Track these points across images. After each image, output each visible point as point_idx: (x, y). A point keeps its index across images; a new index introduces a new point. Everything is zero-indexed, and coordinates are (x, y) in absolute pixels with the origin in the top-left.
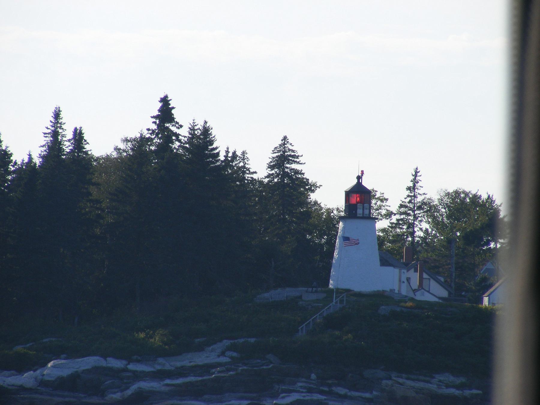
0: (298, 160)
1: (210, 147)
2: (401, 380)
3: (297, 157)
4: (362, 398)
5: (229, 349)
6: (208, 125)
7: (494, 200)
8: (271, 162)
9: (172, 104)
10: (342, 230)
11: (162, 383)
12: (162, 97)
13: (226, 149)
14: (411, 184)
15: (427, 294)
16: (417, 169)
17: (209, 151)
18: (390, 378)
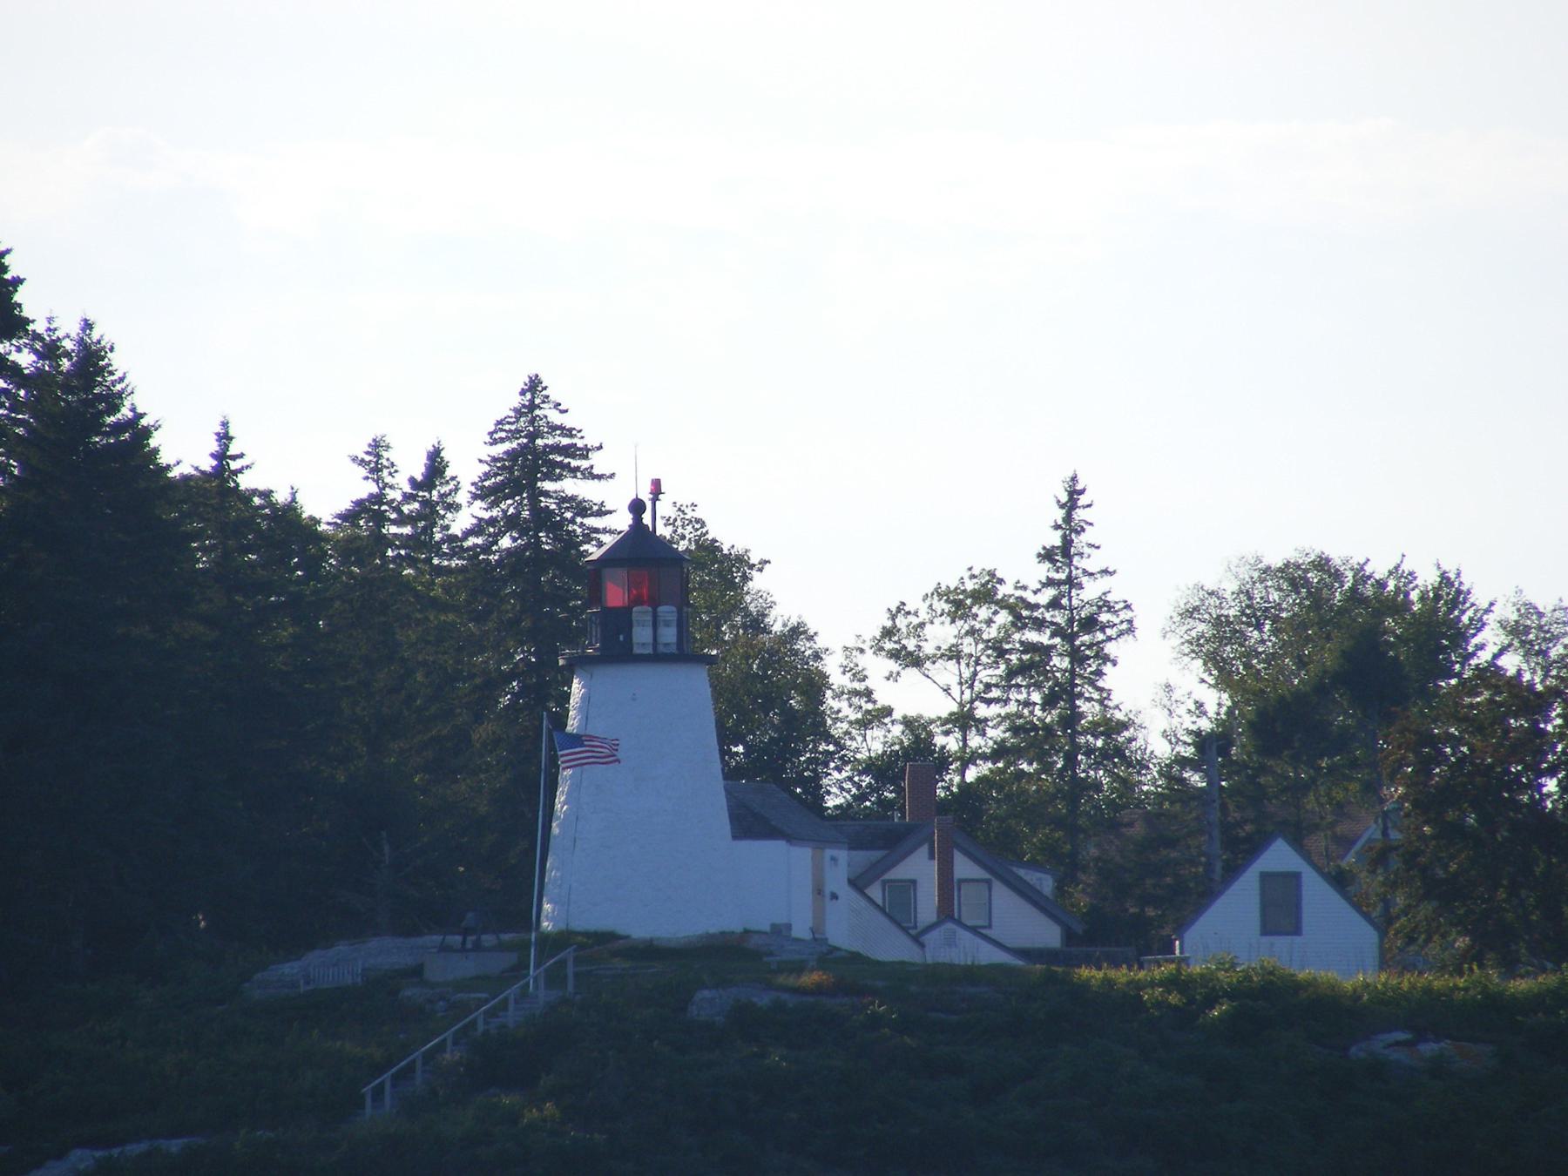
0: (584, 464)
1: (111, 420)
3: (584, 453)
6: (95, 336)
7: (1464, 588)
8: (487, 476)
10: (580, 709)
13: (219, 429)
14: (1055, 539)
15: (965, 937)
16: (1074, 479)
17: (107, 434)
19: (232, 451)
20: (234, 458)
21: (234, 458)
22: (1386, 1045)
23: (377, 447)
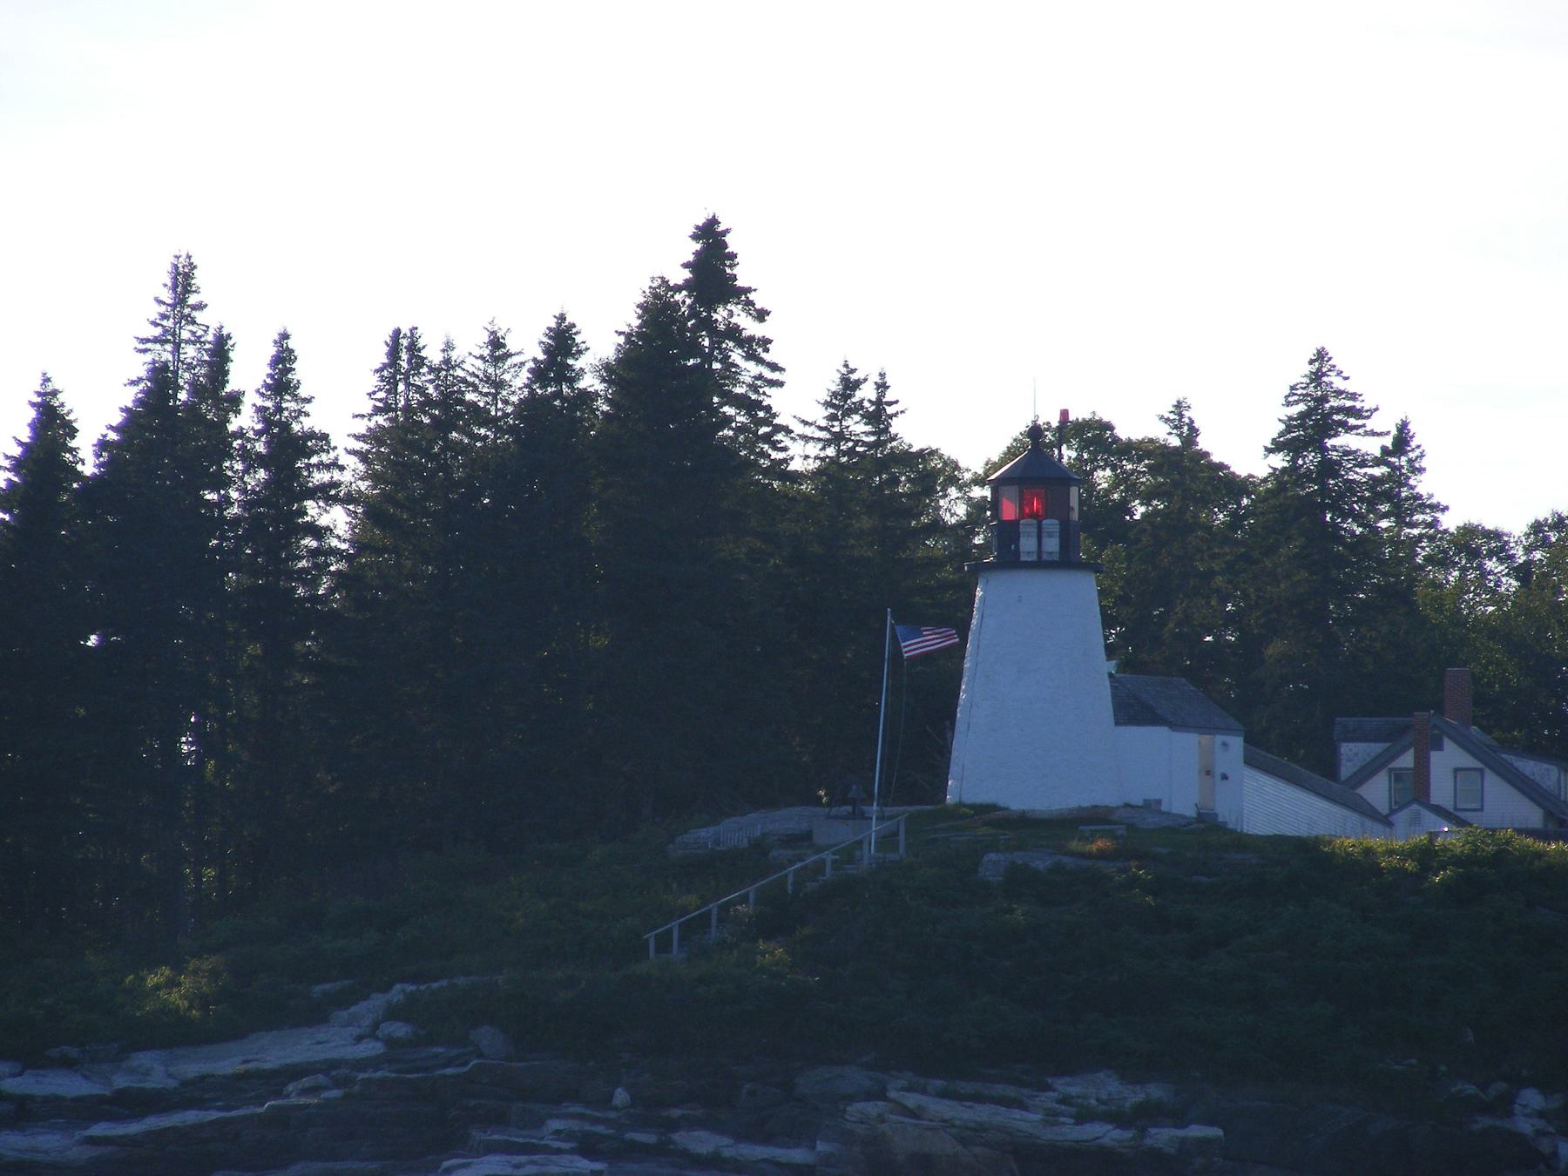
2: (912, 1100)
4: (778, 1164)
5: (393, 1013)
8: (1281, 434)
9: (733, 243)
11: (79, 1134)
18: (881, 1095)
19: (888, 398)
20: (890, 404)
21: (890, 404)
23: (1179, 407)
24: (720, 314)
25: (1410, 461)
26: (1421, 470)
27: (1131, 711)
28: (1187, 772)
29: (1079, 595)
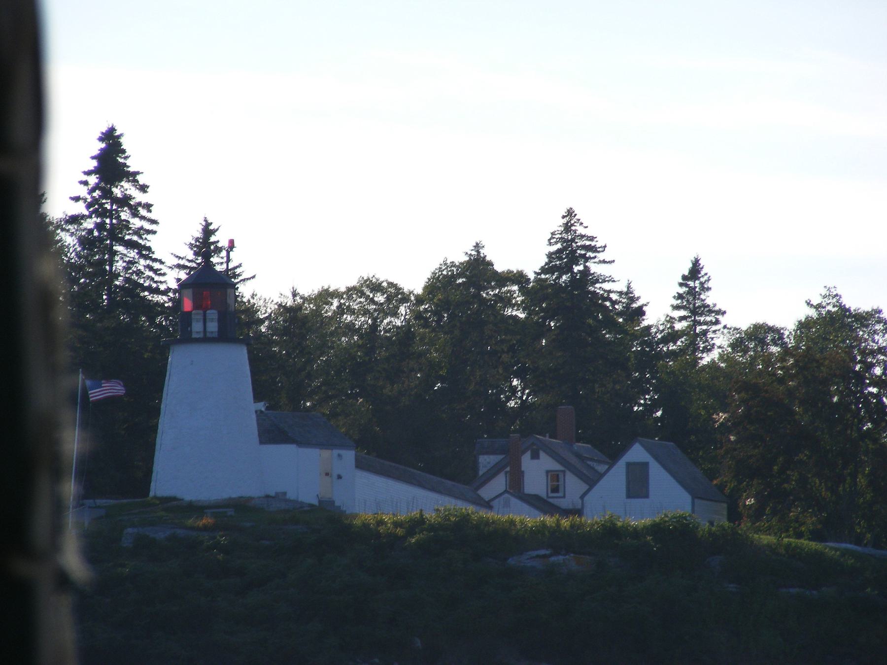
9: (125, 143)
12: (104, 130)
16: (208, 231)
22: (527, 560)
24: (117, 192)
25: (702, 284)
26: (709, 289)
27: (272, 433)
28: (303, 474)
29: (236, 359)
